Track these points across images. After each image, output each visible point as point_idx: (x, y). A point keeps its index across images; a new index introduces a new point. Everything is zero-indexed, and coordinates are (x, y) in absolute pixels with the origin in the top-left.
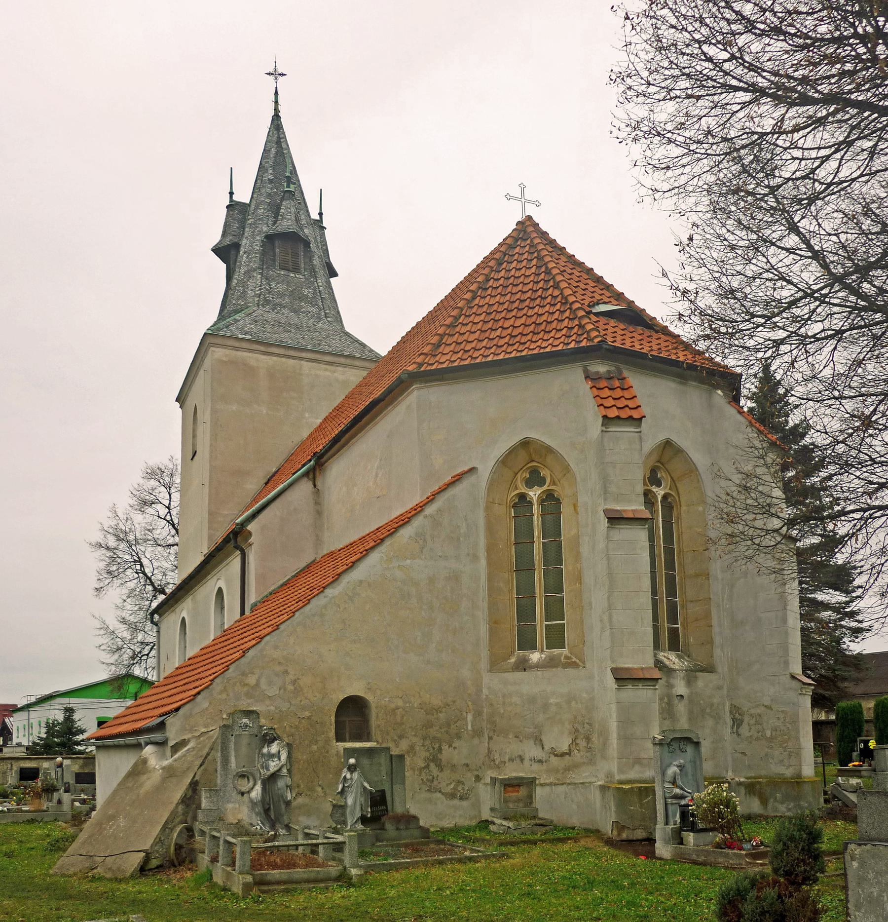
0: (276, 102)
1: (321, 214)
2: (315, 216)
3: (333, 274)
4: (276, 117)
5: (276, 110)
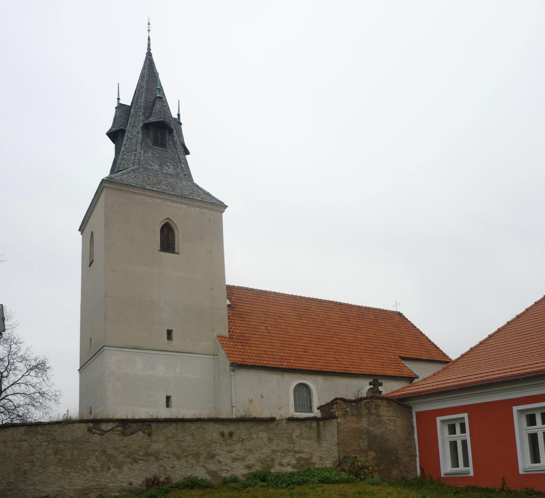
1: (179, 115)
2: (175, 116)
3: (187, 152)
4: (149, 55)
5: (149, 49)
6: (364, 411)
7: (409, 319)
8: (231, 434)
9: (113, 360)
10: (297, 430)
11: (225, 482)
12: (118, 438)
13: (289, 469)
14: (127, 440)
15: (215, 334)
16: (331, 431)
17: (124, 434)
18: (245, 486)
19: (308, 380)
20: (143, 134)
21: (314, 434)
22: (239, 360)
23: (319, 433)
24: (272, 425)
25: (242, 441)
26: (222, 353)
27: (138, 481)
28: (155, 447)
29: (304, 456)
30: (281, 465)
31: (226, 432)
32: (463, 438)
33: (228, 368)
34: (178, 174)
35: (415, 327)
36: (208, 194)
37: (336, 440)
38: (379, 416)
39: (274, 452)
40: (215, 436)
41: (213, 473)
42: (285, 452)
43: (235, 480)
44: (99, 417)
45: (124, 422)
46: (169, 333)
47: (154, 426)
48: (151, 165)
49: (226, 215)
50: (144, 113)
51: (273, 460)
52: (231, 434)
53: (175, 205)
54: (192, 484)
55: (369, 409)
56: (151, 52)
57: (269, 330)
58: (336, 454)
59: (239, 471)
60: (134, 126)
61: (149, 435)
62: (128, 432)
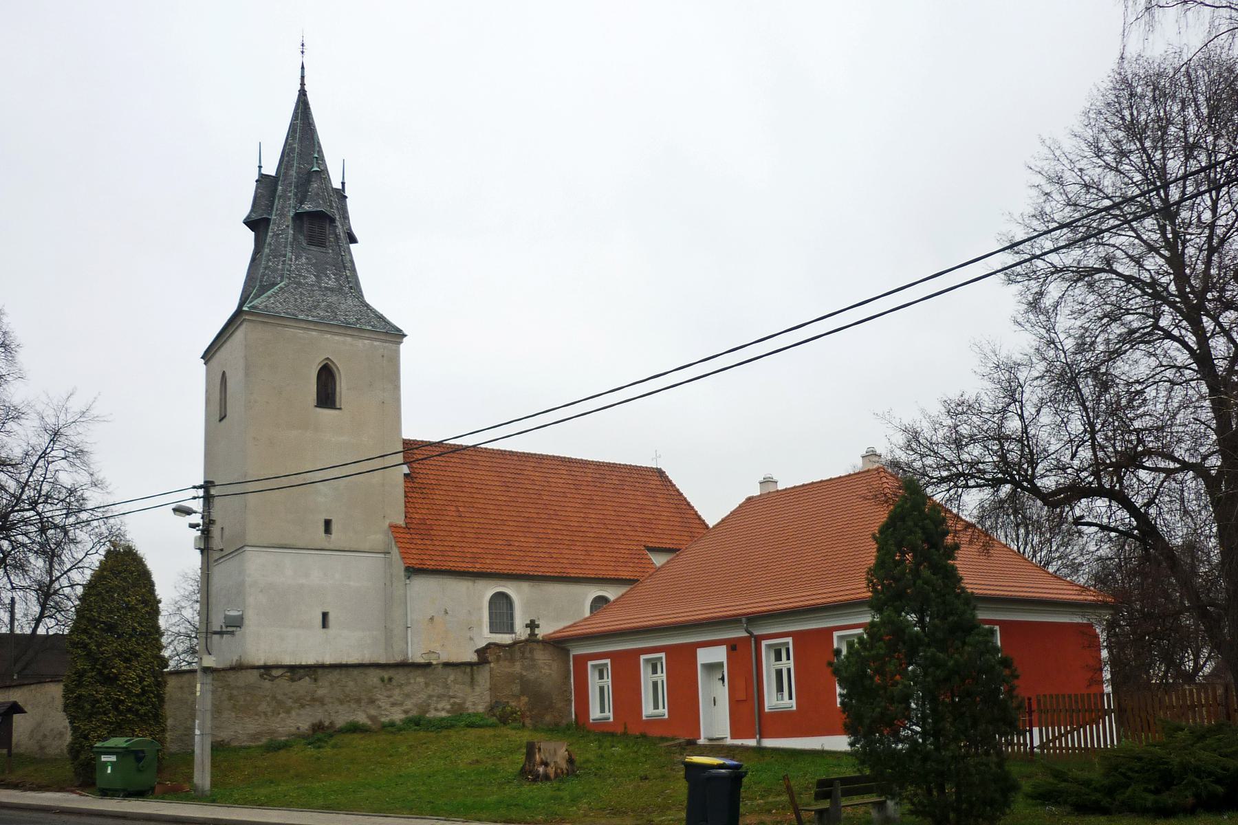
0: (303, 77)
1: (343, 184)
2: (336, 184)
3: (353, 239)
4: (303, 93)
5: (303, 84)
6: (518, 655)
7: (674, 482)
8: (390, 679)
9: (258, 566)
10: (452, 676)
11: (384, 727)
12: (287, 684)
13: (443, 714)
14: (296, 685)
15: (387, 522)
16: (483, 677)
17: (292, 680)
18: (400, 730)
19: (510, 589)
20: (294, 230)
21: (468, 679)
22: (414, 562)
23: (472, 679)
24: (428, 670)
25: (400, 686)
26: (395, 552)
27: (305, 726)
28: (320, 692)
29: (458, 701)
30: (436, 710)
31: (386, 677)
32: (779, 667)
33: (402, 573)
34: (341, 288)
35: (681, 494)
36: (381, 318)
37: (488, 685)
38: (533, 659)
39: (430, 697)
40: (376, 680)
41: (372, 718)
42: (440, 697)
43: (392, 724)
44: (270, 663)
45: (292, 668)
46: (328, 523)
47: (320, 671)
48: (305, 278)
49: (405, 347)
50: (296, 194)
51: (429, 705)
52: (390, 679)
53: (337, 338)
54: (354, 728)
55: (523, 653)
56: (306, 88)
57: (466, 506)
58: (488, 699)
59: (397, 716)
60: (282, 215)
61: (316, 680)
62: (297, 677)
